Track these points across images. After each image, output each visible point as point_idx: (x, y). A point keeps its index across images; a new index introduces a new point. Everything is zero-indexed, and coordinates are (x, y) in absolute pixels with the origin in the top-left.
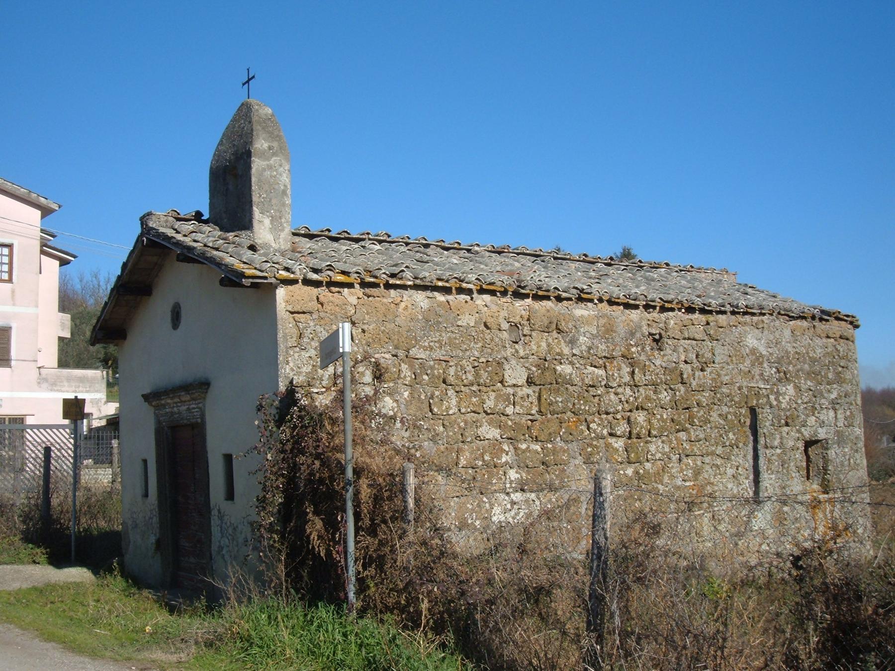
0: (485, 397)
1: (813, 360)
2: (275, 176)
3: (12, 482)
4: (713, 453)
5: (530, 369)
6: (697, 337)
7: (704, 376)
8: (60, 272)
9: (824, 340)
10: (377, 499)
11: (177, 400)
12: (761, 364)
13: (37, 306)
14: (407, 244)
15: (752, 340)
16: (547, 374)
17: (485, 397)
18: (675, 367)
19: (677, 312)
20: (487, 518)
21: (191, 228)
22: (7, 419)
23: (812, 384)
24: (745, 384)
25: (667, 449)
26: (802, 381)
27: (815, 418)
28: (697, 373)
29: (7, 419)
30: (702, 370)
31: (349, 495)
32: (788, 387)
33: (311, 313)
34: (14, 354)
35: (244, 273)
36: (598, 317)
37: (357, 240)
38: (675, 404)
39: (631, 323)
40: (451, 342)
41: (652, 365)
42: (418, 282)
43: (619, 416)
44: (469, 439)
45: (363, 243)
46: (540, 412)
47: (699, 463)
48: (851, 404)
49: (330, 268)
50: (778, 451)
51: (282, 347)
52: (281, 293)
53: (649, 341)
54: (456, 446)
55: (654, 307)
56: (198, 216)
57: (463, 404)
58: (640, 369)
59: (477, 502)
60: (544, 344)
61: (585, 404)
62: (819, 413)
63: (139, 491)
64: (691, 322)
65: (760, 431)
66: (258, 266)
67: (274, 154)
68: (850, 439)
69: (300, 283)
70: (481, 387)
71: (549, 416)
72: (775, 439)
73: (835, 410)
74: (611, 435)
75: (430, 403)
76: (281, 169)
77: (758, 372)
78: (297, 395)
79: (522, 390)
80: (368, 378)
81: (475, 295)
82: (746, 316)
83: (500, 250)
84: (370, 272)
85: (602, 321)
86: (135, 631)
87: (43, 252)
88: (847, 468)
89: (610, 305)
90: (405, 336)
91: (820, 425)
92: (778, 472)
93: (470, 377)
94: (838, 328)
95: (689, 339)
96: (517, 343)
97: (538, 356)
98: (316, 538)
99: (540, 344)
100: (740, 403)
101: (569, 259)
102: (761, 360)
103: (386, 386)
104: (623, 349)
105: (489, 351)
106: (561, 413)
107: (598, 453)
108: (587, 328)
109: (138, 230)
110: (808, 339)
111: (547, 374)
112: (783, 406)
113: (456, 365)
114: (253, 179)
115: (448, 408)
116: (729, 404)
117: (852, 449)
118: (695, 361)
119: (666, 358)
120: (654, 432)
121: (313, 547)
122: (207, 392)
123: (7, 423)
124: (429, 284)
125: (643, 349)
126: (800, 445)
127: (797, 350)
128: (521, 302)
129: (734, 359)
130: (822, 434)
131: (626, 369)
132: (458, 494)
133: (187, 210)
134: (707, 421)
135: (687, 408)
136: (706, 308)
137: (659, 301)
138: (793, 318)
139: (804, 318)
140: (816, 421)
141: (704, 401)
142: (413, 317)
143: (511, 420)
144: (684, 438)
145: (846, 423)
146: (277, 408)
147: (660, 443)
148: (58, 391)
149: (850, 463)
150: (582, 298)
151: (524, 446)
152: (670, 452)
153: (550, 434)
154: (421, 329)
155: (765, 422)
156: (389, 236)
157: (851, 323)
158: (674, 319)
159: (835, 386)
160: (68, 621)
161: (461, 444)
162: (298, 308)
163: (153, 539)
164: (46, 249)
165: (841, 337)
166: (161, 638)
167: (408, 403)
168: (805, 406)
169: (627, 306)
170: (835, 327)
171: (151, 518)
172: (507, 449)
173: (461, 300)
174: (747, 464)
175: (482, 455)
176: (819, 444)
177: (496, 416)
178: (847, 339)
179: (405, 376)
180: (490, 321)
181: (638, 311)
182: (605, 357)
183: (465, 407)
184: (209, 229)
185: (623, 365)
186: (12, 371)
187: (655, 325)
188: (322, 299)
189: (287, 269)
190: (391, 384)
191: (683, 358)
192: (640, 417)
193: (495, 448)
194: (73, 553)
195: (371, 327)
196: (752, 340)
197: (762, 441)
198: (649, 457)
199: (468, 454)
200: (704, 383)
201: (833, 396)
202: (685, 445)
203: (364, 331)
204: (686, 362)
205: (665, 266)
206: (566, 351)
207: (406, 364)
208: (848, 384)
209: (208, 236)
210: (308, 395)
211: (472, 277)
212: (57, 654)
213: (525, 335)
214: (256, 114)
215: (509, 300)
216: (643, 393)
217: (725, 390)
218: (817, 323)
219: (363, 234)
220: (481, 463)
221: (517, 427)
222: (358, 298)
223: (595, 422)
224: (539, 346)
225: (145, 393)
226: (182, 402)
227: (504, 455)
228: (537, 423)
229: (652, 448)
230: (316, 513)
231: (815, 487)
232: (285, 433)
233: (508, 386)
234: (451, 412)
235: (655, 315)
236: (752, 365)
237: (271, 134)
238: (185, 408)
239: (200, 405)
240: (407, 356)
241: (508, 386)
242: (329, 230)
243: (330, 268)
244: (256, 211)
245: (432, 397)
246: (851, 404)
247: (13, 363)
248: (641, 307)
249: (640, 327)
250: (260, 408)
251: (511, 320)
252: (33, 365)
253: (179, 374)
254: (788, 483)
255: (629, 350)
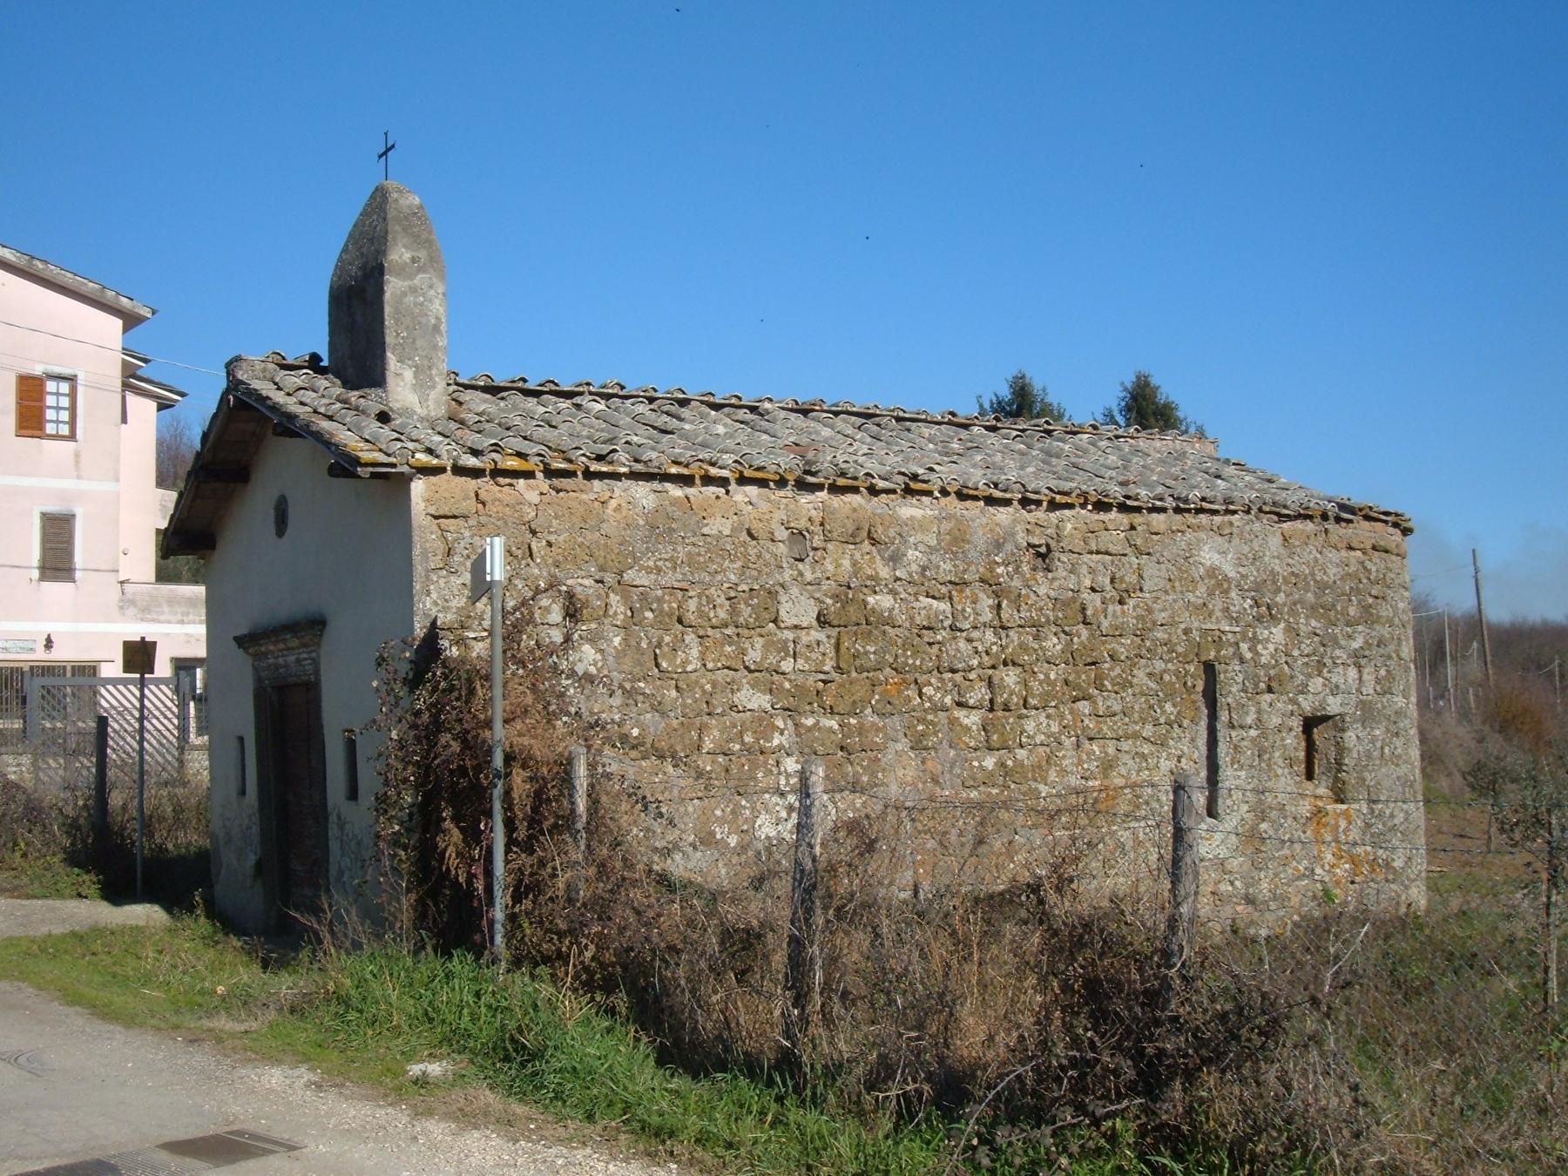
0: (747, 645)
1: (1322, 587)
2: (421, 304)
3: (61, 772)
4: (1136, 736)
5: (823, 602)
6: (1112, 549)
7: (1123, 612)
8: (159, 420)
9: (1344, 553)
10: (539, 797)
11: (281, 646)
12: (1226, 592)
13: (118, 480)
14: (651, 400)
15: (1210, 555)
16: (851, 609)
17: (747, 645)
18: (1073, 597)
19: (1078, 509)
20: (747, 833)
21: (299, 382)
22: (69, 668)
23: (1318, 625)
24: (1196, 624)
25: (1055, 728)
26: (1302, 620)
27: (1321, 680)
28: (1111, 608)
29: (69, 668)
30: (1121, 602)
31: (497, 792)
32: (1274, 630)
33: (465, 517)
34: (79, 559)
35: (359, 458)
36: (939, 519)
37: (568, 395)
38: (1071, 657)
39: (998, 529)
40: (691, 561)
41: (1032, 595)
42: (639, 467)
43: (972, 676)
44: (719, 710)
45: (578, 400)
46: (838, 668)
47: (1111, 751)
48: (1390, 657)
49: (496, 448)
50: (1253, 733)
51: (419, 569)
52: (418, 487)
53: (1028, 556)
54: (697, 721)
55: (1038, 503)
56: (314, 362)
57: (710, 656)
58: (1010, 601)
59: (731, 806)
60: (846, 563)
61: (915, 654)
62: (1329, 672)
63: (233, 787)
64: (1102, 526)
65: (1221, 701)
66: (383, 447)
67: (420, 270)
68: (1384, 716)
69: (449, 472)
70: (740, 630)
71: (854, 674)
72: (1247, 713)
73: (1359, 667)
74: (959, 704)
75: (656, 655)
76: (432, 292)
77: (1220, 605)
78: (441, 642)
79: (808, 634)
80: (556, 616)
81: (733, 487)
82: (1201, 516)
83: (805, 407)
84: (564, 452)
85: (946, 526)
86: (202, 992)
87: (126, 386)
88: (1378, 762)
89: (961, 500)
90: (616, 551)
91: (1331, 690)
92: (1251, 766)
93: (722, 614)
94: (1368, 534)
95: (1098, 552)
96: (801, 560)
97: (836, 581)
98: (454, 855)
99: (840, 562)
100: (1186, 656)
101: (925, 421)
102: (1225, 586)
103: (584, 628)
104: (981, 570)
105: (755, 573)
106: (875, 670)
107: (935, 733)
108: (920, 537)
109: (223, 384)
110: (1314, 552)
111: (851, 609)
112: (1263, 660)
113: (699, 596)
114: (387, 310)
115: (685, 662)
116: (1165, 657)
117: (1388, 730)
118: (1109, 588)
119: (1056, 584)
120: (1032, 701)
121: (448, 869)
122: (321, 635)
123: (69, 674)
124: (656, 471)
125: (1017, 570)
126: (1295, 724)
127: (1294, 569)
128: (811, 497)
129: (1177, 584)
130: (1334, 706)
131: (987, 602)
132: (700, 794)
133: (296, 352)
134: (1126, 684)
135: (1094, 664)
136: (1129, 502)
137: (1047, 492)
138: (1283, 518)
139: (1310, 517)
140: (1324, 685)
141: (1123, 653)
142: (630, 522)
143: (790, 681)
144: (1087, 711)
145: (1378, 688)
146: (411, 662)
147: (1042, 718)
148: (153, 620)
149: (1383, 753)
150: (912, 488)
151: (810, 722)
152: (1060, 733)
153: (854, 702)
154: (642, 540)
155: (1231, 685)
156: (623, 388)
157: (1396, 525)
158: (1072, 521)
159: (1360, 628)
160: (110, 978)
161: (706, 718)
162: (445, 510)
163: (251, 859)
164: (131, 380)
165: (1374, 548)
166: (243, 1001)
167: (620, 654)
168: (1306, 660)
169: (990, 501)
170: (1363, 531)
171: (249, 828)
172: (782, 726)
173: (709, 494)
174: (1196, 753)
175: (741, 734)
176: (1330, 722)
177: (766, 676)
178: (1387, 551)
179: (616, 613)
180: (757, 527)
181: (1010, 509)
182: (950, 582)
183: (713, 661)
184: (326, 383)
185: (982, 595)
186: (77, 588)
187: (1038, 530)
188: (483, 495)
189: (430, 451)
190: (593, 626)
191: (1088, 583)
192: (1010, 677)
193: (762, 721)
194: (139, 884)
195: (561, 538)
196: (1210, 555)
197: (1223, 716)
198: (1024, 740)
199: (716, 733)
200: (1123, 623)
201: (1356, 645)
202: (1087, 721)
203: (550, 544)
204: (1093, 589)
205: (1090, 429)
206: (884, 572)
207: (617, 594)
208: (1384, 625)
209: (323, 396)
210: (460, 642)
211: (728, 459)
212: (80, 1021)
213: (815, 549)
214: (393, 206)
215: (790, 494)
216: (1016, 638)
217: (1160, 634)
218: (1331, 526)
219: (580, 385)
220: (737, 747)
221: (800, 691)
222: (542, 494)
223: (931, 684)
224: (838, 566)
225: (237, 634)
226: (288, 649)
227: (776, 734)
228: (833, 686)
229: (1030, 726)
230: (456, 819)
231: (1322, 791)
232: (423, 698)
233: (787, 628)
234: (689, 668)
235: (1040, 514)
236: (1209, 595)
237: (416, 237)
238: (292, 658)
239: (314, 655)
240: (619, 582)
241: (787, 628)
242: (524, 380)
243: (496, 448)
244: (391, 358)
245: (659, 646)
246: (1390, 657)
247: (78, 575)
248: (1015, 503)
249: (1014, 535)
250: (381, 661)
251: (792, 525)
252: (112, 577)
253: (286, 607)
254: (1269, 784)
255: (992, 571)
